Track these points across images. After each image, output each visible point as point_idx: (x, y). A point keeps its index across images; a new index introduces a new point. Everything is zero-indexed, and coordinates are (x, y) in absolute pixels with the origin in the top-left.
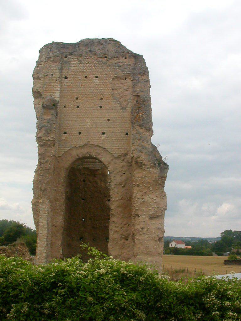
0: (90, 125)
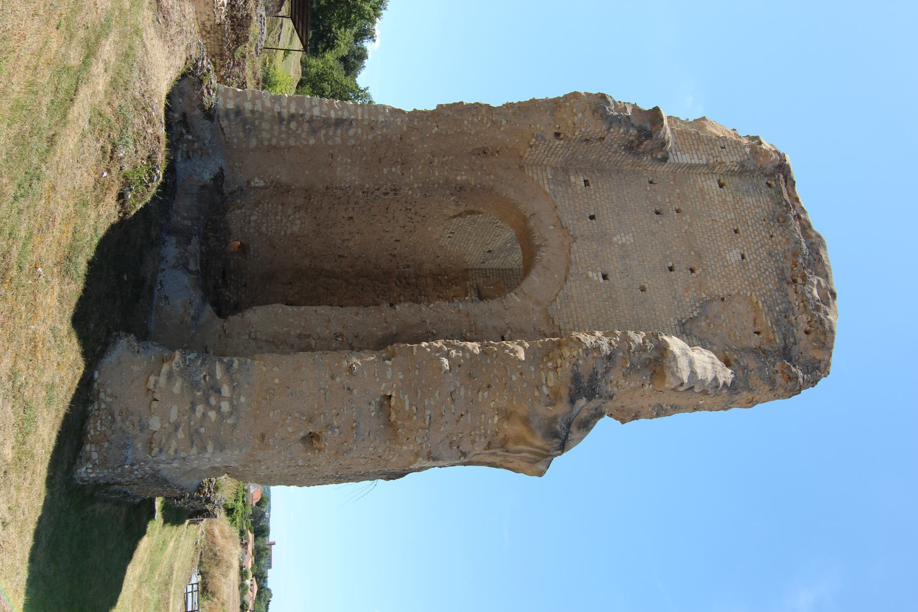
0: (620, 242)
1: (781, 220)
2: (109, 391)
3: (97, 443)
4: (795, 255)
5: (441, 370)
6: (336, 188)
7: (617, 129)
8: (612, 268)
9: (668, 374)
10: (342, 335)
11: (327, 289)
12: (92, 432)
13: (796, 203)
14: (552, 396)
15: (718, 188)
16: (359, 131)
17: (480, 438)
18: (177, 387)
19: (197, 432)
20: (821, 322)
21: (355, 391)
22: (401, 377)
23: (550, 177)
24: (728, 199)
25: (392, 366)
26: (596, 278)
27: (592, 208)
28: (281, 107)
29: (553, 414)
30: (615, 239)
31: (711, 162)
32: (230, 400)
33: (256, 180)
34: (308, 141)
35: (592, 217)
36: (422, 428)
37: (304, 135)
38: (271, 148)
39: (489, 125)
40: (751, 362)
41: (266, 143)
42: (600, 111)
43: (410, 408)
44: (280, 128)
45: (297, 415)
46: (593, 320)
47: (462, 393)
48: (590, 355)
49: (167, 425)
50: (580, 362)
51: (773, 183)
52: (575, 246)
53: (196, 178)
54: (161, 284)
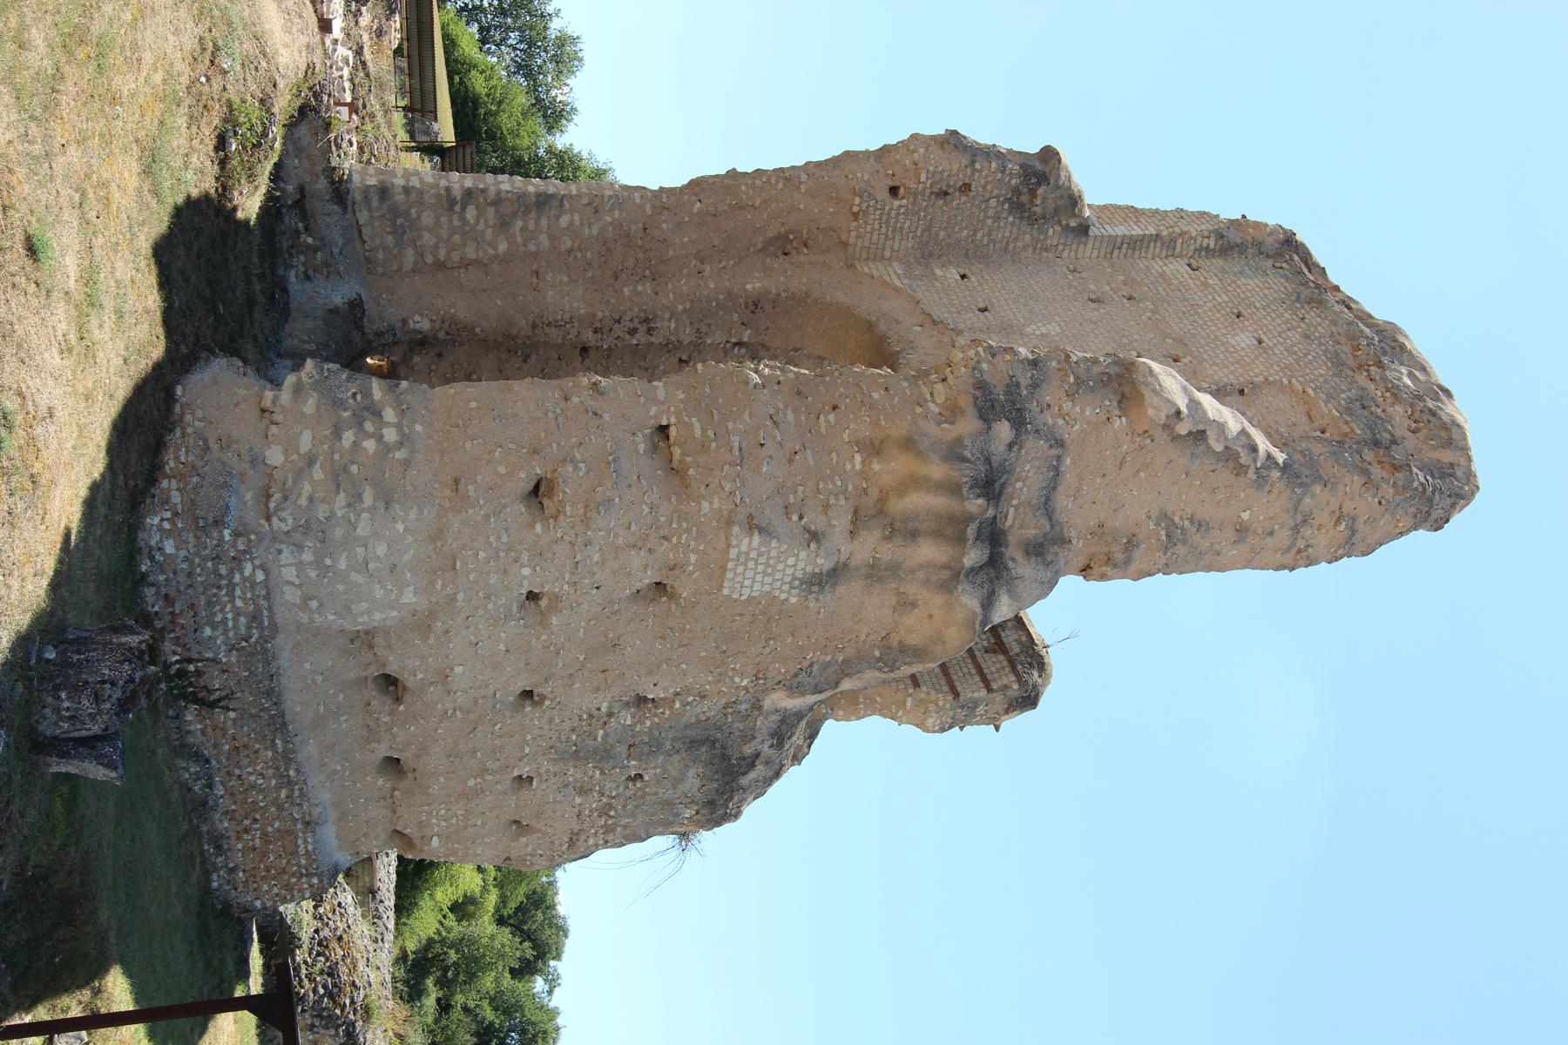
2: (199, 414)
3: (180, 477)
6: (549, 324)
9: (1146, 393)
12: (172, 464)
16: (576, 217)
17: (837, 499)
18: (310, 406)
19: (345, 469)
21: (607, 417)
29: (954, 435)
32: (399, 427)
33: (417, 318)
34: (495, 247)
37: (489, 234)
38: (441, 266)
41: (429, 259)
44: (450, 221)
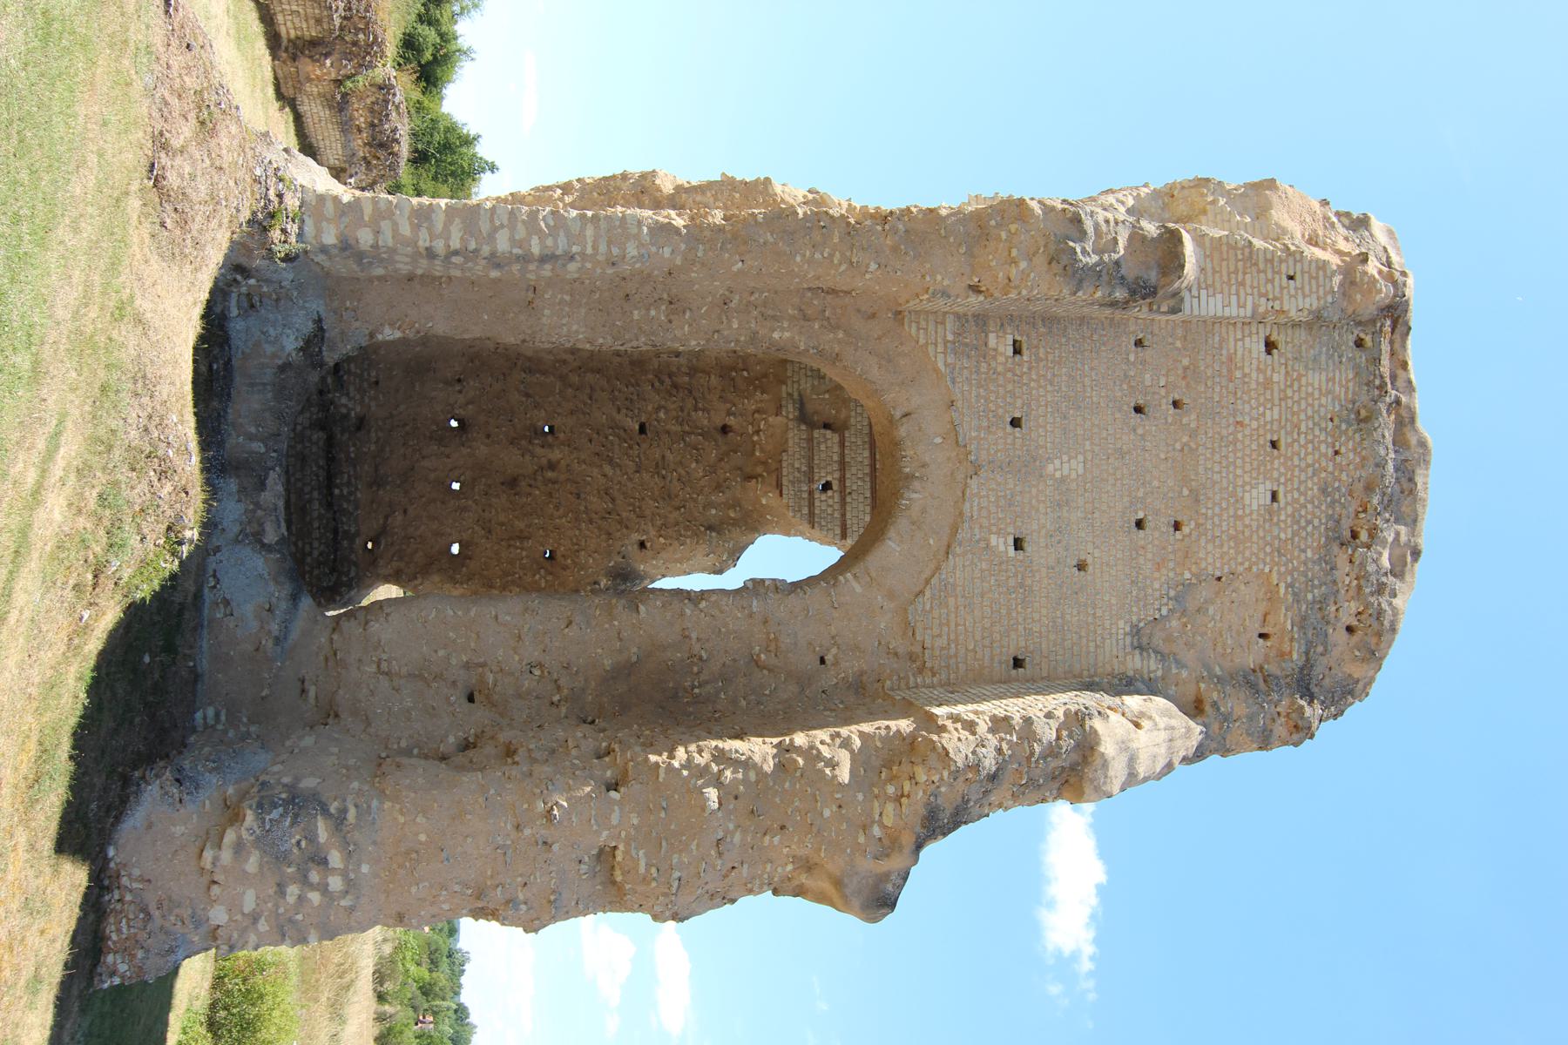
0: (1058, 475)
1: (1364, 420)
2: (136, 872)
3: (127, 952)
4: (1369, 488)
5: (703, 810)
7: (1091, 289)
8: (1035, 527)
10: (541, 665)
11: (527, 395)
12: (114, 937)
13: (1400, 372)
14: (886, 842)
15: (1263, 355)
18: (252, 864)
20: (1380, 613)
21: (555, 847)
22: (635, 821)
23: (950, 337)
24: (1276, 378)
25: (620, 803)
26: (1002, 548)
27: (1019, 403)
28: (432, 237)
30: (1050, 468)
31: (1261, 310)
32: (344, 873)
35: (1015, 423)
36: (666, 895)
39: (843, 268)
40: (1237, 704)
42: (1065, 260)
43: (647, 870)
45: (457, 888)
46: (984, 628)
47: (737, 838)
48: (961, 779)
49: (239, 917)
50: (943, 789)
51: (1368, 339)
52: (973, 483)
53: (269, 349)
54: (214, 576)
